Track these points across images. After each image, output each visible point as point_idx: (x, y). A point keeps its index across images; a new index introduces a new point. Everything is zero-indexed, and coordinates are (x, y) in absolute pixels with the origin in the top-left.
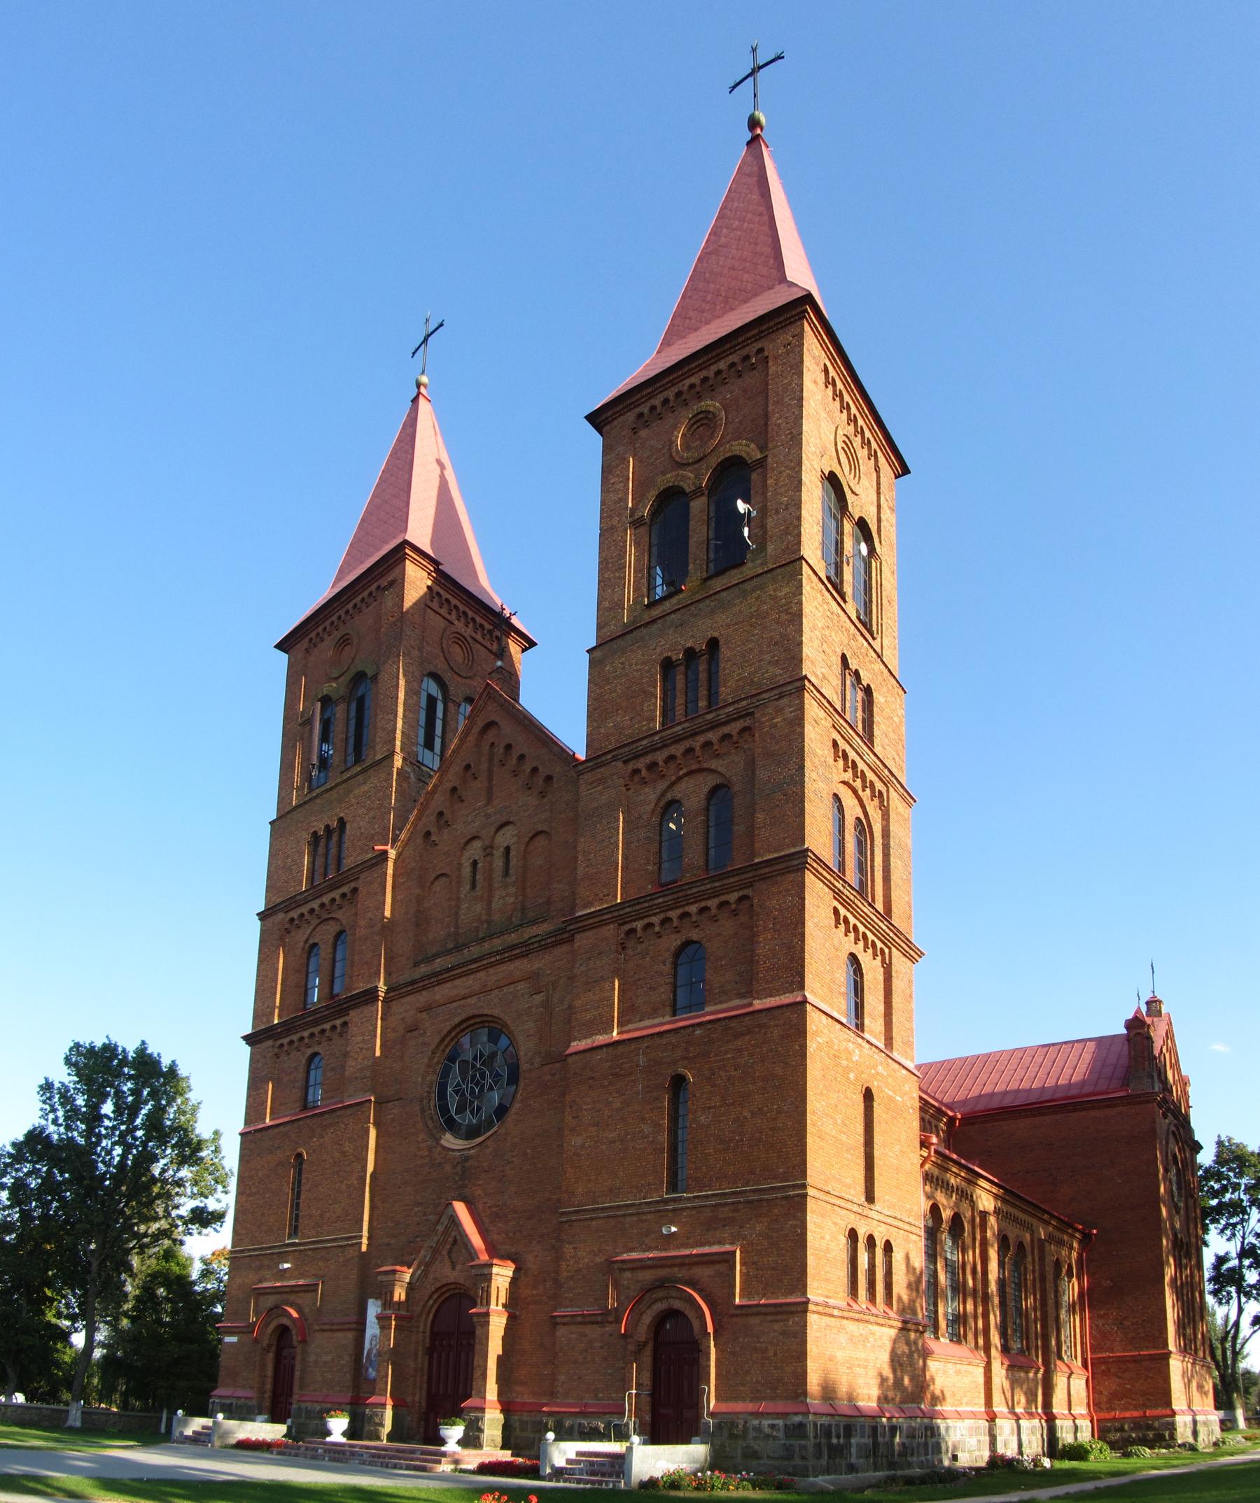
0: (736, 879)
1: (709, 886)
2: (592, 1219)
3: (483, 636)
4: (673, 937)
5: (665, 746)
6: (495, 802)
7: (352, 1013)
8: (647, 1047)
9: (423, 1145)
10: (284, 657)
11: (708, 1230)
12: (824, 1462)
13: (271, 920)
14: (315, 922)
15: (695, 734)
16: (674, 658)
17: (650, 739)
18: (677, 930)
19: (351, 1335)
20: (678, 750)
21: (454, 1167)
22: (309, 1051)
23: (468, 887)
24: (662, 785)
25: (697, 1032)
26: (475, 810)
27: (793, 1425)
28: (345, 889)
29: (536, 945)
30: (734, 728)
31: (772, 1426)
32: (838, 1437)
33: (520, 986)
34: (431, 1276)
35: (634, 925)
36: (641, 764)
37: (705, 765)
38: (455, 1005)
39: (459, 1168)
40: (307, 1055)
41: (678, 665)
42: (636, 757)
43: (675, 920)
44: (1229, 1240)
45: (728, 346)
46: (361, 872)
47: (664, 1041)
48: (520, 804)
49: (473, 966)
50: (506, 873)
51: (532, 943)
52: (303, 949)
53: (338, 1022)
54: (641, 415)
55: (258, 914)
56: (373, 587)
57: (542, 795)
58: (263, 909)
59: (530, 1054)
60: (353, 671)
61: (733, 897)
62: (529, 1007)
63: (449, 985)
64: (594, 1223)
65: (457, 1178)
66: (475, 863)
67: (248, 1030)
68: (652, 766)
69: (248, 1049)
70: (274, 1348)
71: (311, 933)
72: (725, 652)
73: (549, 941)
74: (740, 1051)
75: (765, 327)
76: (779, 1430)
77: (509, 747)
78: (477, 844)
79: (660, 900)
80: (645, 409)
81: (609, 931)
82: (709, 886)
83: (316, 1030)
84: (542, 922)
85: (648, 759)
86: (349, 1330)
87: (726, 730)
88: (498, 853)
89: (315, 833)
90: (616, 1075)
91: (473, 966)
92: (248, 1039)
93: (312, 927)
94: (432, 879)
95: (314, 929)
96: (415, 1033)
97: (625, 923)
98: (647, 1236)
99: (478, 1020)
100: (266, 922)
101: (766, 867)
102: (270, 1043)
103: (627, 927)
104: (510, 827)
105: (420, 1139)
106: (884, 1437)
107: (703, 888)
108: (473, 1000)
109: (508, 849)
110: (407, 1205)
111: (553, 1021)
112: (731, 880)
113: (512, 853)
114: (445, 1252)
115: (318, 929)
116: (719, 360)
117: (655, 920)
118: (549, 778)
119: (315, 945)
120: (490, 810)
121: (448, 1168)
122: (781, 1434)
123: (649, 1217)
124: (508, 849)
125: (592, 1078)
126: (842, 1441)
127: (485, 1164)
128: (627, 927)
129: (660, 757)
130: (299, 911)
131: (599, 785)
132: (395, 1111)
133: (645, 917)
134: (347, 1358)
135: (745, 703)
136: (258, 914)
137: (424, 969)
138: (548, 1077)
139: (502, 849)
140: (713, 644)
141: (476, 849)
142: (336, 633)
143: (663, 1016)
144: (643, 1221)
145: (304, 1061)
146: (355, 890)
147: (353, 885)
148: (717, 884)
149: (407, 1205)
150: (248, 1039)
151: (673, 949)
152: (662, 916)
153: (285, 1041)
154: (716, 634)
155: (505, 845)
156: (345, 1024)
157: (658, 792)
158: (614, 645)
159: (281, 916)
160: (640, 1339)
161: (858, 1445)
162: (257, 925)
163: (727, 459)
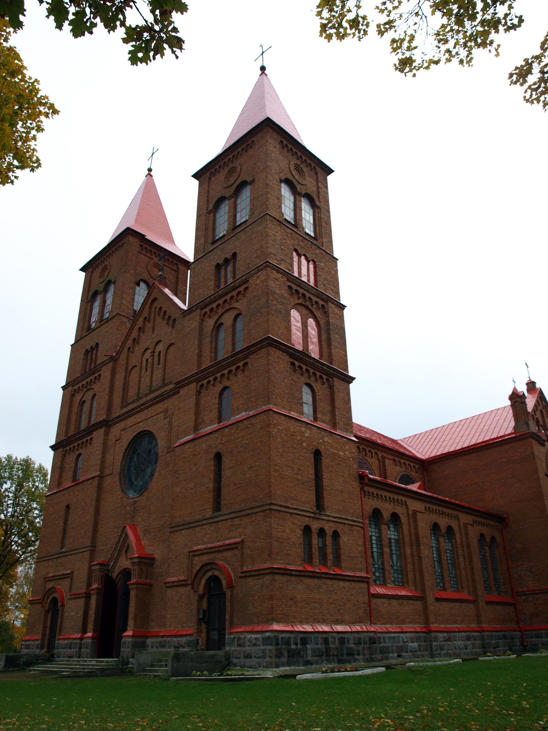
0: (241, 355)
1: (231, 360)
2: (183, 530)
3: (147, 252)
4: (219, 385)
5: (216, 300)
6: (155, 332)
7: (94, 433)
8: (206, 440)
9: (119, 497)
10: (83, 274)
11: (230, 531)
12: (284, 660)
13: (67, 390)
14: (85, 390)
15: (227, 294)
16: (220, 263)
17: (209, 298)
18: (221, 382)
19: (83, 600)
20: (221, 301)
21: (131, 507)
22: (78, 453)
23: (144, 371)
24: (216, 317)
25: (226, 430)
26: (148, 336)
27: (266, 638)
28: (97, 375)
29: (166, 395)
30: (242, 289)
31: (256, 639)
32: (296, 644)
33: (160, 415)
34: (118, 565)
35: (203, 382)
36: (207, 309)
37: (232, 306)
38: (134, 426)
39: (132, 508)
40: (77, 454)
41: (222, 266)
42: (206, 307)
43: (219, 377)
44: (353, 37)
45: (241, 142)
46: (102, 366)
47: (213, 436)
48: (165, 332)
49: (142, 407)
50: (159, 364)
51: (164, 395)
52: (79, 403)
53: (89, 438)
54: (212, 173)
55: (62, 387)
56: (117, 246)
57: (173, 327)
58: (64, 384)
59: (162, 448)
60: (107, 280)
61: (241, 364)
62: (163, 425)
63: (133, 417)
64: (183, 531)
65: (131, 513)
66: (147, 360)
67: (53, 442)
68: (211, 310)
69: (52, 452)
70: (51, 610)
71: (83, 396)
72: (239, 258)
73: (171, 393)
74: (243, 437)
75: (253, 133)
76: (259, 641)
77: (161, 308)
78: (149, 351)
79: (212, 369)
80: (213, 170)
81: (193, 386)
82: (231, 360)
83: (80, 442)
84: (169, 384)
85: (210, 307)
86: (82, 597)
87: (239, 290)
88: (156, 354)
89: (87, 350)
90: (194, 455)
91: (142, 407)
92: (52, 447)
93: (83, 393)
94: (131, 368)
95: (84, 394)
96: (119, 441)
97: (199, 382)
98: (205, 537)
99: (144, 433)
100: (65, 391)
101: (253, 347)
102: (61, 449)
103: (200, 383)
104: (161, 343)
105: (118, 494)
106: (334, 644)
107: (228, 361)
108: (141, 424)
109: (160, 352)
110: (111, 528)
111: (172, 431)
112: (239, 356)
113: (162, 354)
114: (124, 552)
115: (86, 393)
116: (239, 148)
117: (211, 379)
118: (174, 320)
119: (84, 401)
120: (153, 336)
121: (128, 508)
122: (260, 643)
123: (206, 526)
124: (160, 352)
125: (184, 457)
126: (299, 646)
127: (143, 505)
128: (200, 383)
129: (214, 305)
130: (78, 386)
131: (191, 320)
132: (109, 480)
133: (207, 378)
134: (80, 613)
135: (245, 277)
136: (62, 387)
137: (124, 410)
138: (169, 459)
139: (158, 353)
140: (234, 255)
141: (148, 354)
142: (103, 264)
143: (215, 424)
144: (203, 529)
145: (75, 458)
146: (100, 375)
147: (99, 373)
148: (234, 358)
149: (111, 528)
150: (52, 447)
151: (219, 392)
152: (214, 377)
153: (68, 448)
154: (235, 251)
155: (159, 351)
156: (91, 439)
157: (215, 320)
158: (199, 261)
159: (70, 388)
160: (200, 593)
161: (312, 649)
162: (61, 392)
163: (241, 182)
